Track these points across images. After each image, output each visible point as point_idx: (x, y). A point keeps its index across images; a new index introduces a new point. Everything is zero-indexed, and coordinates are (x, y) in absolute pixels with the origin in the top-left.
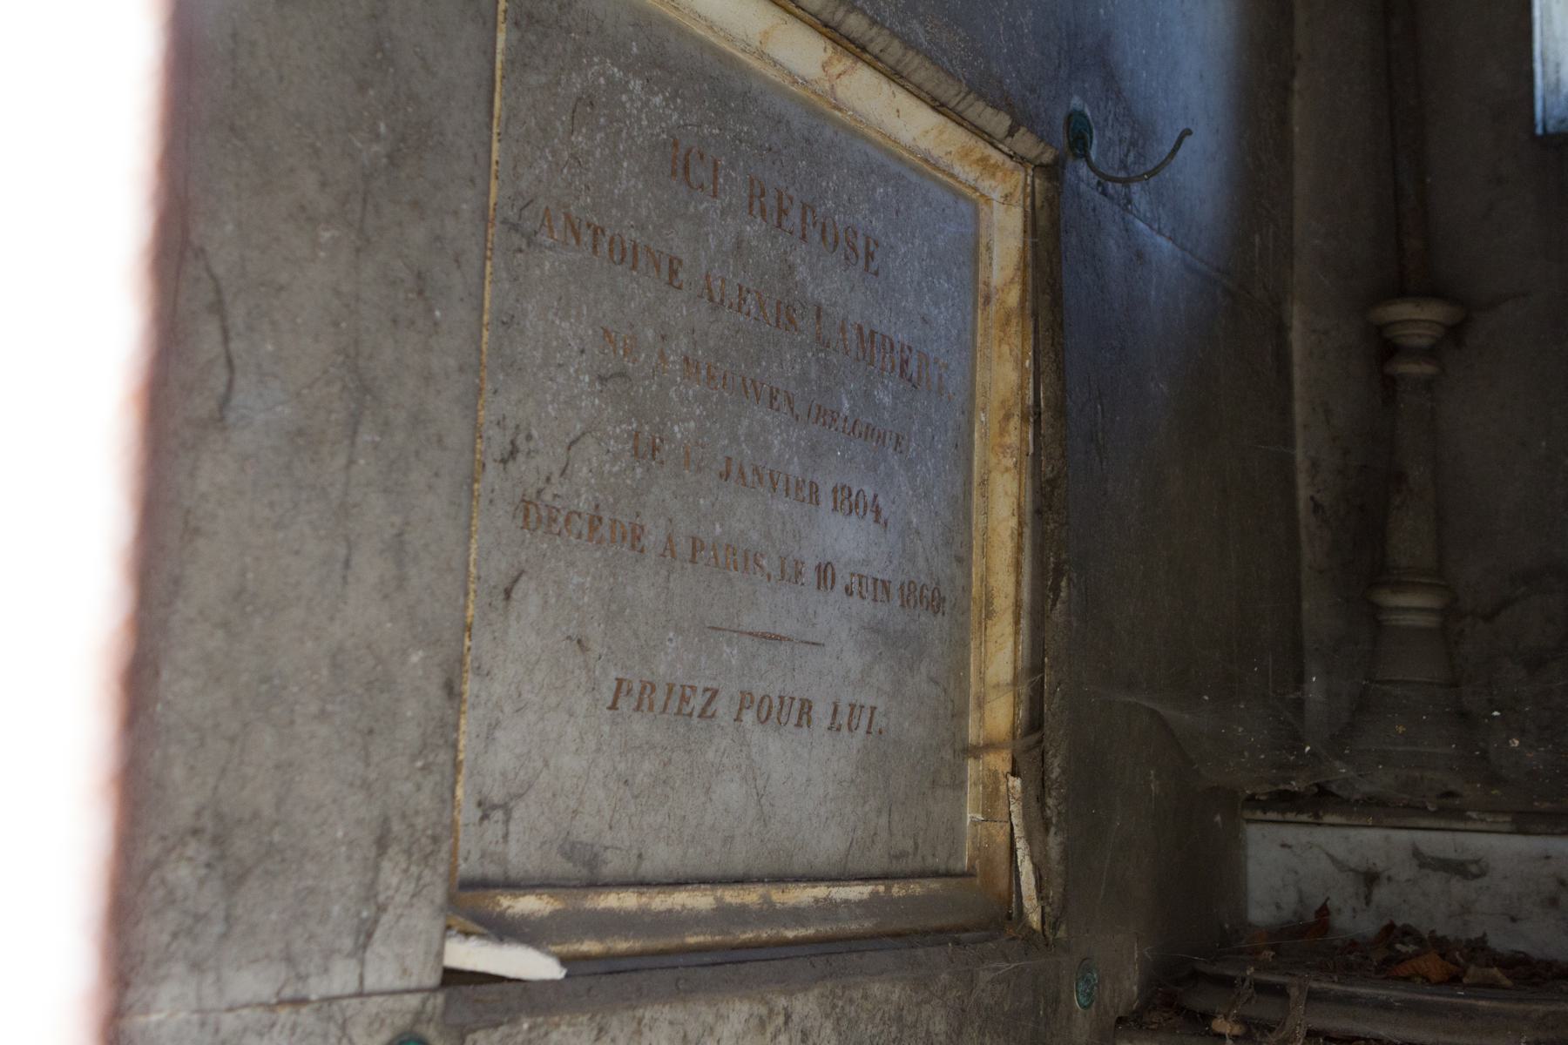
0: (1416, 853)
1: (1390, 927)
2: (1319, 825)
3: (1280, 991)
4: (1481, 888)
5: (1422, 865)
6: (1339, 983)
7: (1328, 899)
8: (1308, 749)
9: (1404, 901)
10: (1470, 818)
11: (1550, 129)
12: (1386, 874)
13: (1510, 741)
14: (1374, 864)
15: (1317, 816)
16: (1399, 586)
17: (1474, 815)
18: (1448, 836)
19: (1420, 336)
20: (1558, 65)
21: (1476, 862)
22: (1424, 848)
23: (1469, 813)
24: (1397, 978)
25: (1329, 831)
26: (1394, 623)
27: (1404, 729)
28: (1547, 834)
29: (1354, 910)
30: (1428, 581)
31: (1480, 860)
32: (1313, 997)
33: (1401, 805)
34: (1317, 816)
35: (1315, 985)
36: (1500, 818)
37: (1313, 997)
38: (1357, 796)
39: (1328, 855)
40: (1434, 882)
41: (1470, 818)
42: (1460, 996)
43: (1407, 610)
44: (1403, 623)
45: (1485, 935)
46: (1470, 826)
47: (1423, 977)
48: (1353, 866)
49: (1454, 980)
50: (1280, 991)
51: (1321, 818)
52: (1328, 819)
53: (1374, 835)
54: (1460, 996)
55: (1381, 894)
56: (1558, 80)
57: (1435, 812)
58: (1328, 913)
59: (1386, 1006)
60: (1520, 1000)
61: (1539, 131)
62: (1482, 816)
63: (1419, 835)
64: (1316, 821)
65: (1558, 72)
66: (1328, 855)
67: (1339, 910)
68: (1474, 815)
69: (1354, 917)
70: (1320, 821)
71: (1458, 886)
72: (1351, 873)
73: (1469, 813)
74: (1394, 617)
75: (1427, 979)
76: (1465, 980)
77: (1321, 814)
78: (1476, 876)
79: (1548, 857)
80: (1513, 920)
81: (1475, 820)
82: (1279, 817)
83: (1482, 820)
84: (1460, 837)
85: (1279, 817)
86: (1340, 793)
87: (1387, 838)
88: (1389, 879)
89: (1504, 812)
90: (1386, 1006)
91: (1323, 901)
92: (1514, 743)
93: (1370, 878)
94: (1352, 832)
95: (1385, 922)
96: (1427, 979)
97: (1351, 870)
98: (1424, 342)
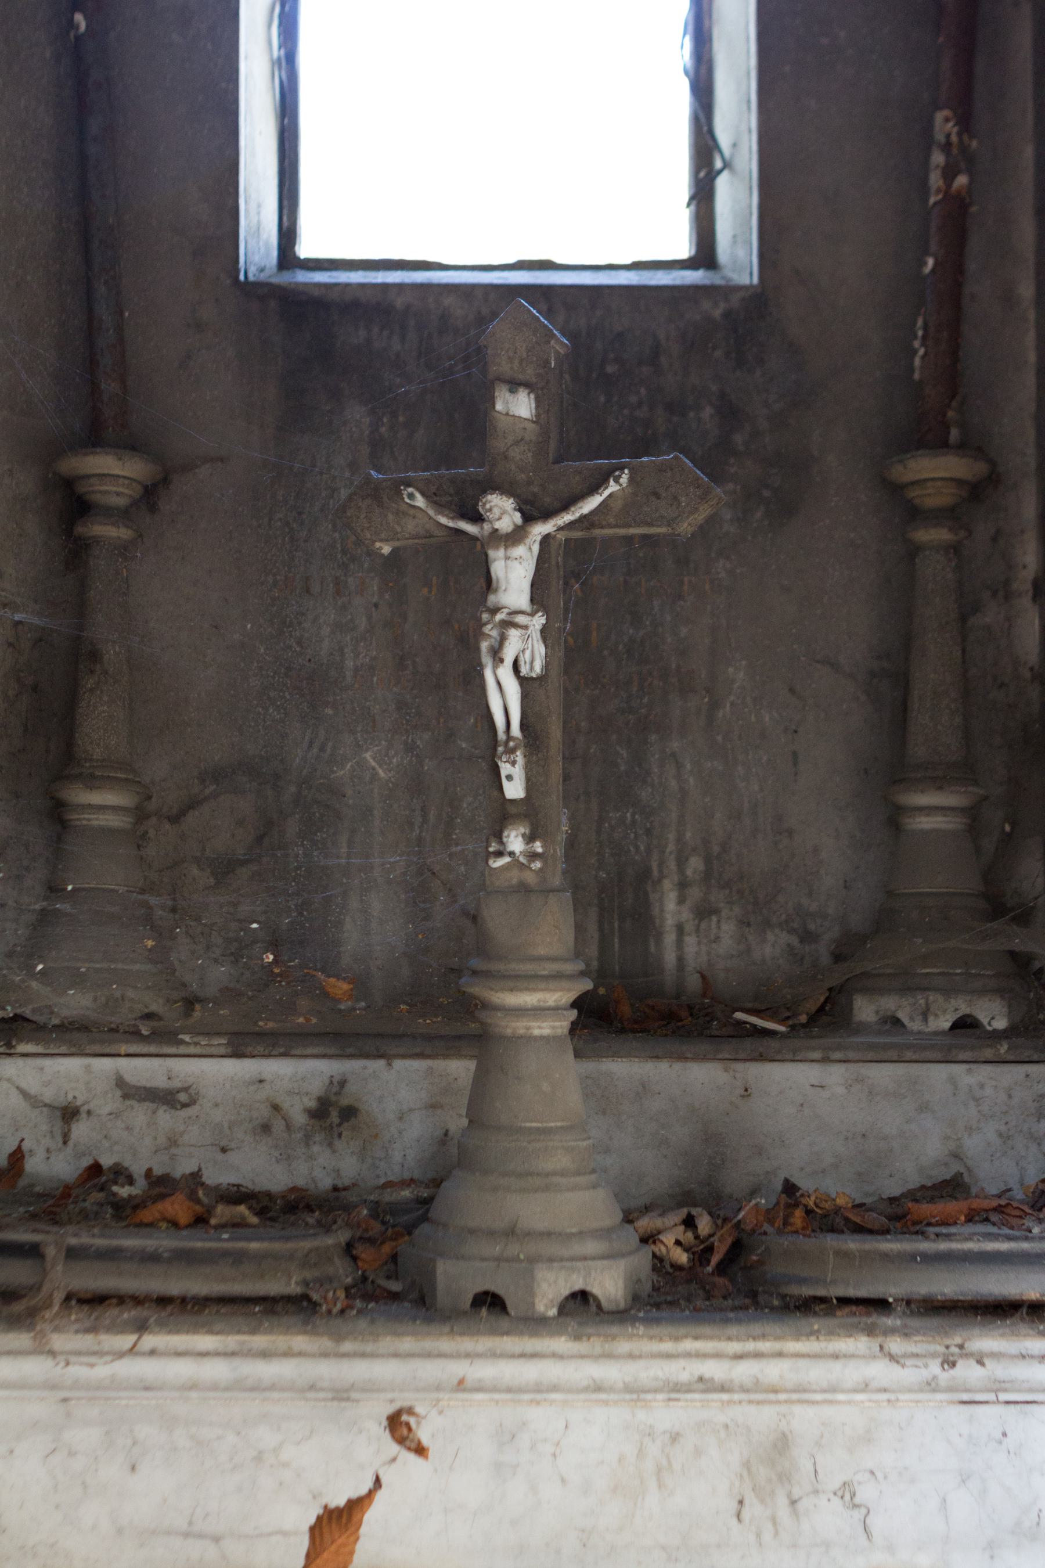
0: (120, 1082)
1: (95, 1169)
2: (10, 1055)
3: (32, 1252)
4: (190, 1118)
5: (125, 1096)
6: (102, 1236)
7: (22, 1140)
8: (40, 967)
9: (106, 1137)
10: (182, 1042)
11: (251, 278)
12: (85, 1108)
13: (264, 956)
14: (75, 1097)
15: (9, 1045)
16: (92, 782)
17: (187, 1038)
18: (156, 1062)
19: (118, 494)
20: (259, 206)
21: (186, 1089)
22: (128, 1078)
23: (180, 1036)
24: (141, 1225)
25: (20, 1062)
26: (85, 822)
27: (154, 943)
28: (263, 1056)
29: (48, 1151)
30: (123, 776)
31: (190, 1087)
32: (73, 1254)
33: (106, 1029)
34: (9, 1045)
35: (73, 1241)
36: (216, 1041)
37: (73, 1254)
38: (56, 1021)
39: (18, 1088)
40: (139, 1114)
41: (182, 1042)
42: (225, 1240)
43: (102, 808)
44: (95, 823)
45: (200, 1170)
46: (182, 1050)
47: (169, 1221)
48: (47, 1101)
49: (200, 1221)
50: (32, 1252)
51: (14, 1047)
52: (23, 1048)
53: (73, 1065)
54: (225, 1240)
55: (80, 1130)
56: (259, 223)
57: (147, 1037)
58: (23, 1157)
59: (152, 1258)
60: (288, 1239)
61: (242, 277)
62: (196, 1039)
63: (123, 1063)
64: (8, 1051)
65: (259, 213)
66: (18, 1088)
67: (31, 1151)
68: (187, 1038)
69: (48, 1158)
70: (12, 1051)
71: (165, 1118)
72: (45, 1109)
73: (180, 1036)
74: (86, 816)
75: (174, 1224)
76: (213, 1221)
77: (14, 1043)
78: (185, 1106)
79: (261, 1081)
80: (224, 1150)
81: (188, 1044)
82: (39, 1049)
83: (196, 1044)
84: (171, 1062)
85: (39, 1049)
86: (34, 1018)
87: (88, 1069)
88: (89, 1112)
89: (218, 1034)
90: (152, 1258)
91: (17, 1143)
92: (268, 957)
93: (69, 1114)
94: (47, 1062)
95: (87, 1162)
96: (174, 1224)
97: (46, 1105)
98: (121, 502)
